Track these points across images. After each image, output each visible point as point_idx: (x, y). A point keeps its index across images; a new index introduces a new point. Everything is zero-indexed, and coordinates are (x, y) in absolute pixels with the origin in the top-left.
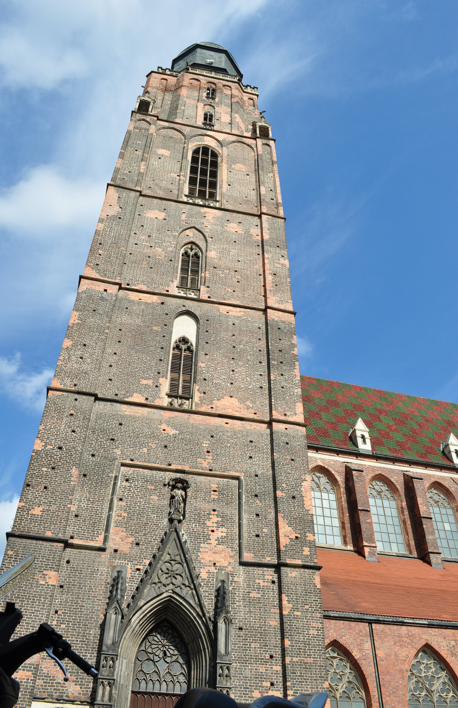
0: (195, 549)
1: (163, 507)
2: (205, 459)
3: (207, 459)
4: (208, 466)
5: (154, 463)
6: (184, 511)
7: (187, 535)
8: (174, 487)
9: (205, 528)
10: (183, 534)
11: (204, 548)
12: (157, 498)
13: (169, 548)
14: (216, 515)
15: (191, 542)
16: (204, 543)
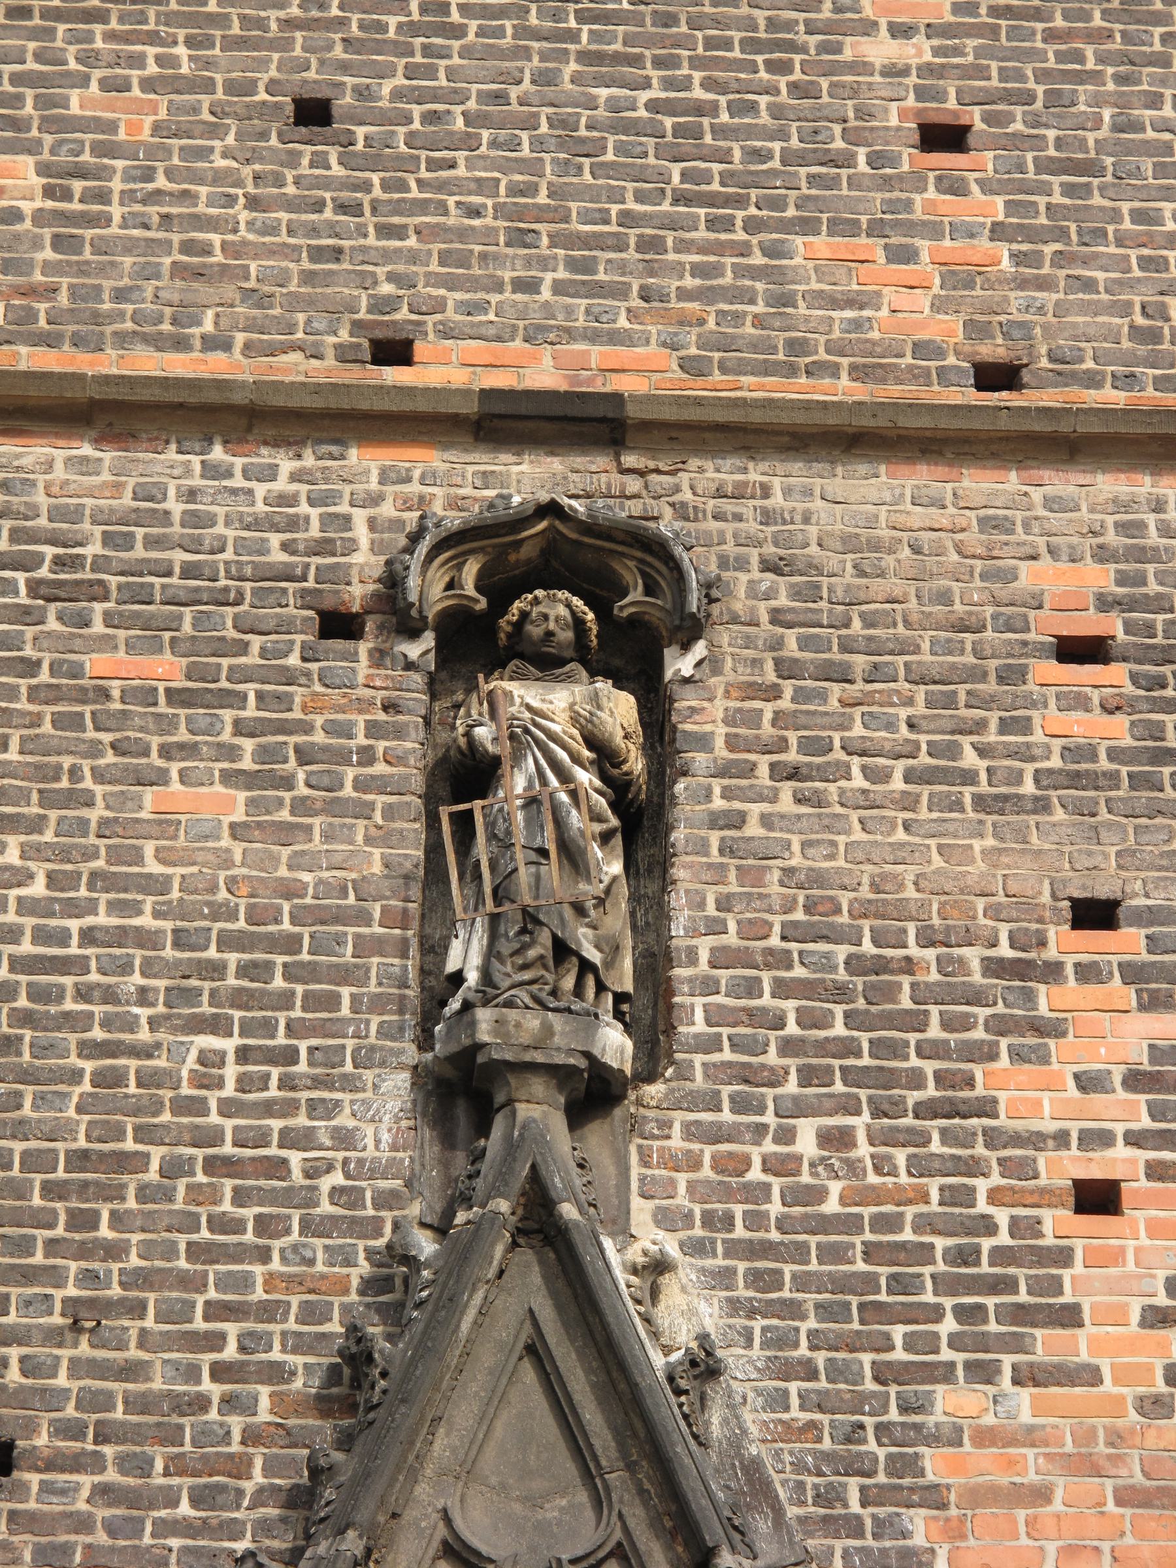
0: (861, 1468)
1: (340, 917)
2: (899, 236)
3: (934, 230)
4: (949, 329)
5: (158, 342)
6: (655, 965)
7: (724, 1278)
8: (474, 645)
9: (974, 1168)
10: (659, 1266)
11: (985, 1437)
12: (237, 805)
13: (466, 1471)
14: (1132, 974)
15: (787, 1371)
16: (983, 1373)
